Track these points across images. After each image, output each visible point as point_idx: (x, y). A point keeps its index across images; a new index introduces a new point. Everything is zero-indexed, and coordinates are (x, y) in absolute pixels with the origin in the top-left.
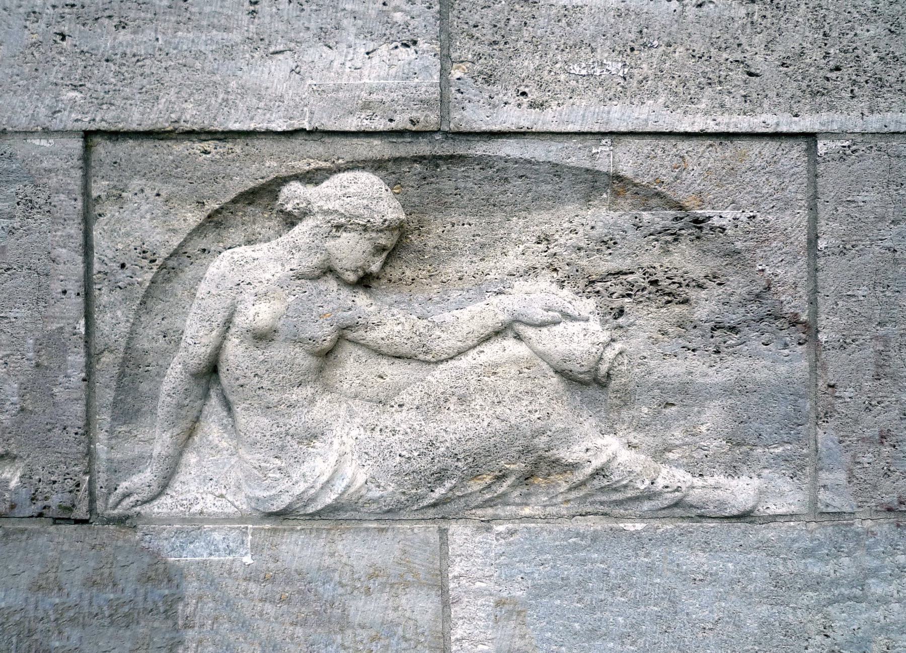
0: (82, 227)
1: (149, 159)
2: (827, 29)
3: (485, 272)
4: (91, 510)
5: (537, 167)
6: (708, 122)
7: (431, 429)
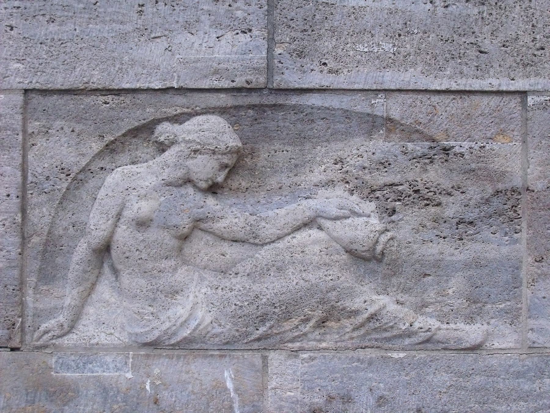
0: (21, 152)
1: (68, 108)
2: (534, 22)
3: (298, 183)
4: (22, 342)
5: (333, 112)
6: (452, 83)
7: (256, 288)
